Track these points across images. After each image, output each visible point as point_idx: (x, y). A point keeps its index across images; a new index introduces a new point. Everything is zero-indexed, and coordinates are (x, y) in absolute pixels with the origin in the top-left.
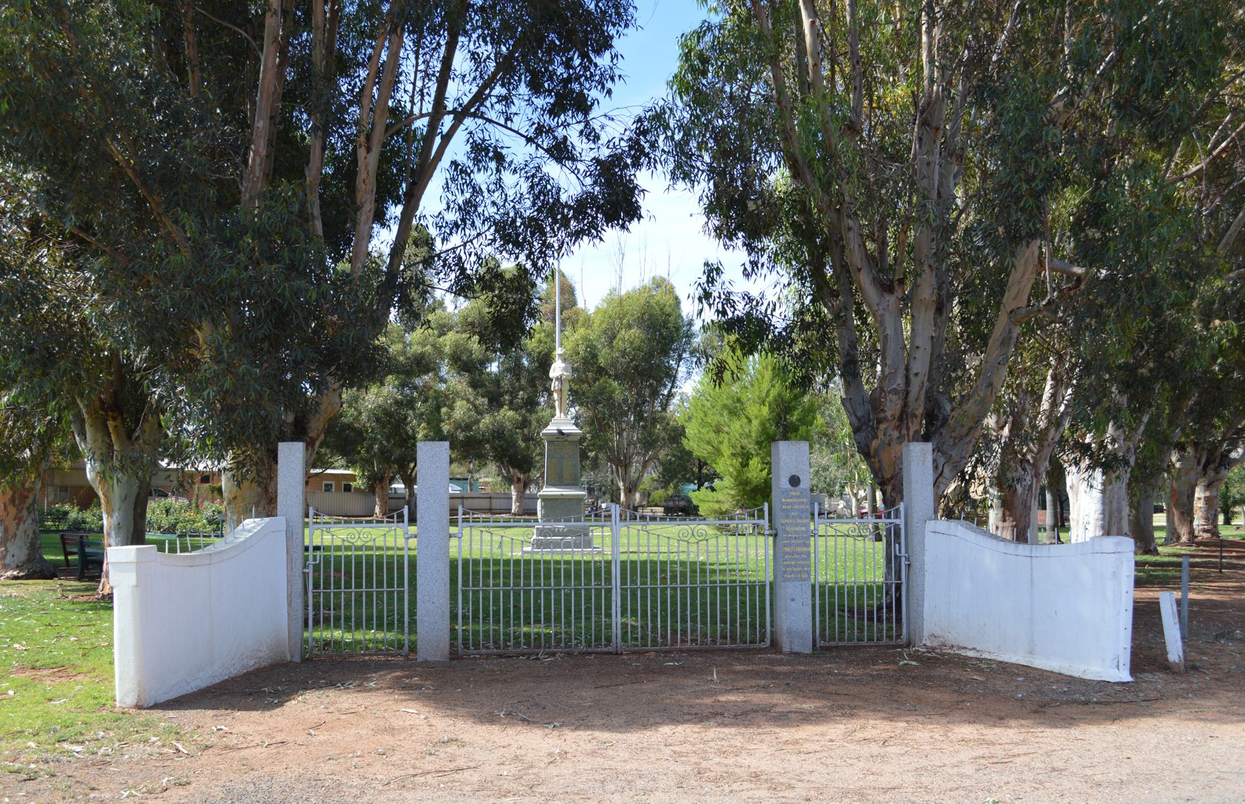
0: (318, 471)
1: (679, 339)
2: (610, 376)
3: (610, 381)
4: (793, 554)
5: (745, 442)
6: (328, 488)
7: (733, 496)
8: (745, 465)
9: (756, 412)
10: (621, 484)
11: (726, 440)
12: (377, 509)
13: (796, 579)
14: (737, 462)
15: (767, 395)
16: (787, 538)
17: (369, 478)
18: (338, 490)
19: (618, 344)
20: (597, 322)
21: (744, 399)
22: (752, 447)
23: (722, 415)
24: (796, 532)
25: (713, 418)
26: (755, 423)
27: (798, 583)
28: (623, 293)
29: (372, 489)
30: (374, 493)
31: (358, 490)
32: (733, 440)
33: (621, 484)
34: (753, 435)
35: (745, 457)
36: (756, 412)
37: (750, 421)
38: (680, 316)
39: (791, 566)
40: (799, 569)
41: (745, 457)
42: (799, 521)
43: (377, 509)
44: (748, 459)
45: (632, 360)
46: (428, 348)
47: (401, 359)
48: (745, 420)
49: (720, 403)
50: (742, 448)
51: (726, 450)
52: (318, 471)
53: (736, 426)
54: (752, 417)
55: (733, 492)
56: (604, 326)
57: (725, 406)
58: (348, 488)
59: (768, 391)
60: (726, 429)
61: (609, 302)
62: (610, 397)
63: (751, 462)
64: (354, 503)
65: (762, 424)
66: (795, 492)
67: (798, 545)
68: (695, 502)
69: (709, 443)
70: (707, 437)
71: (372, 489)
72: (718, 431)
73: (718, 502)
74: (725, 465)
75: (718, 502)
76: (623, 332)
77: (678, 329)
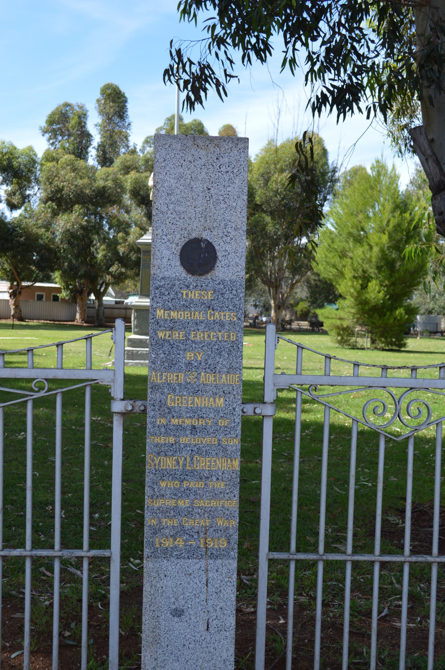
0: (29, 284)
1: (325, 182)
2: (265, 212)
3: (264, 215)
4: (184, 475)
5: (366, 266)
6: (40, 298)
7: (354, 314)
8: (364, 287)
9: (377, 240)
10: (272, 302)
11: (349, 263)
12: (78, 316)
13: (191, 553)
14: (358, 284)
15: (388, 225)
16: (168, 430)
17: (72, 291)
18: (48, 299)
19: (273, 185)
20: (255, 167)
21: (367, 228)
22: (372, 271)
23: (347, 242)
24: (196, 413)
25: (338, 245)
26: (376, 249)
27: (195, 565)
28: (279, 144)
29: (73, 300)
30: (76, 302)
31: (63, 300)
32: (356, 264)
33: (272, 302)
34: (374, 260)
35: (365, 279)
36: (377, 240)
37: (371, 248)
38: (326, 163)
39: (178, 512)
40: (205, 522)
41: (365, 279)
42: (207, 378)
43: (78, 316)
44: (369, 281)
45: (283, 199)
46: (109, 184)
47: (87, 191)
48: (366, 247)
49: (346, 231)
50: (364, 271)
51: (349, 274)
52: (29, 284)
53: (359, 252)
54: (373, 244)
55: (353, 311)
56: (261, 170)
57: (350, 234)
58: (56, 299)
59: (389, 221)
60: (350, 254)
61: (267, 150)
62: (264, 229)
63: (370, 284)
64: (61, 311)
65: (382, 250)
66: (197, 291)
67: (198, 451)
68: (321, 319)
69: (334, 266)
70: (332, 261)
71: (73, 300)
72: (343, 255)
73: (341, 319)
74: (346, 287)
75: (341, 319)
76: (276, 175)
77: (324, 174)
